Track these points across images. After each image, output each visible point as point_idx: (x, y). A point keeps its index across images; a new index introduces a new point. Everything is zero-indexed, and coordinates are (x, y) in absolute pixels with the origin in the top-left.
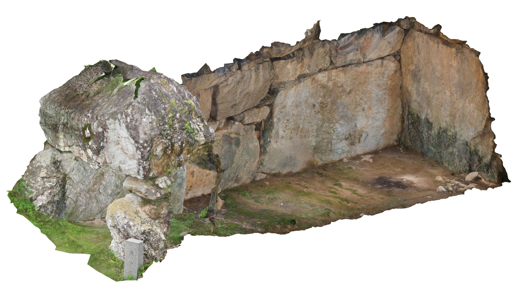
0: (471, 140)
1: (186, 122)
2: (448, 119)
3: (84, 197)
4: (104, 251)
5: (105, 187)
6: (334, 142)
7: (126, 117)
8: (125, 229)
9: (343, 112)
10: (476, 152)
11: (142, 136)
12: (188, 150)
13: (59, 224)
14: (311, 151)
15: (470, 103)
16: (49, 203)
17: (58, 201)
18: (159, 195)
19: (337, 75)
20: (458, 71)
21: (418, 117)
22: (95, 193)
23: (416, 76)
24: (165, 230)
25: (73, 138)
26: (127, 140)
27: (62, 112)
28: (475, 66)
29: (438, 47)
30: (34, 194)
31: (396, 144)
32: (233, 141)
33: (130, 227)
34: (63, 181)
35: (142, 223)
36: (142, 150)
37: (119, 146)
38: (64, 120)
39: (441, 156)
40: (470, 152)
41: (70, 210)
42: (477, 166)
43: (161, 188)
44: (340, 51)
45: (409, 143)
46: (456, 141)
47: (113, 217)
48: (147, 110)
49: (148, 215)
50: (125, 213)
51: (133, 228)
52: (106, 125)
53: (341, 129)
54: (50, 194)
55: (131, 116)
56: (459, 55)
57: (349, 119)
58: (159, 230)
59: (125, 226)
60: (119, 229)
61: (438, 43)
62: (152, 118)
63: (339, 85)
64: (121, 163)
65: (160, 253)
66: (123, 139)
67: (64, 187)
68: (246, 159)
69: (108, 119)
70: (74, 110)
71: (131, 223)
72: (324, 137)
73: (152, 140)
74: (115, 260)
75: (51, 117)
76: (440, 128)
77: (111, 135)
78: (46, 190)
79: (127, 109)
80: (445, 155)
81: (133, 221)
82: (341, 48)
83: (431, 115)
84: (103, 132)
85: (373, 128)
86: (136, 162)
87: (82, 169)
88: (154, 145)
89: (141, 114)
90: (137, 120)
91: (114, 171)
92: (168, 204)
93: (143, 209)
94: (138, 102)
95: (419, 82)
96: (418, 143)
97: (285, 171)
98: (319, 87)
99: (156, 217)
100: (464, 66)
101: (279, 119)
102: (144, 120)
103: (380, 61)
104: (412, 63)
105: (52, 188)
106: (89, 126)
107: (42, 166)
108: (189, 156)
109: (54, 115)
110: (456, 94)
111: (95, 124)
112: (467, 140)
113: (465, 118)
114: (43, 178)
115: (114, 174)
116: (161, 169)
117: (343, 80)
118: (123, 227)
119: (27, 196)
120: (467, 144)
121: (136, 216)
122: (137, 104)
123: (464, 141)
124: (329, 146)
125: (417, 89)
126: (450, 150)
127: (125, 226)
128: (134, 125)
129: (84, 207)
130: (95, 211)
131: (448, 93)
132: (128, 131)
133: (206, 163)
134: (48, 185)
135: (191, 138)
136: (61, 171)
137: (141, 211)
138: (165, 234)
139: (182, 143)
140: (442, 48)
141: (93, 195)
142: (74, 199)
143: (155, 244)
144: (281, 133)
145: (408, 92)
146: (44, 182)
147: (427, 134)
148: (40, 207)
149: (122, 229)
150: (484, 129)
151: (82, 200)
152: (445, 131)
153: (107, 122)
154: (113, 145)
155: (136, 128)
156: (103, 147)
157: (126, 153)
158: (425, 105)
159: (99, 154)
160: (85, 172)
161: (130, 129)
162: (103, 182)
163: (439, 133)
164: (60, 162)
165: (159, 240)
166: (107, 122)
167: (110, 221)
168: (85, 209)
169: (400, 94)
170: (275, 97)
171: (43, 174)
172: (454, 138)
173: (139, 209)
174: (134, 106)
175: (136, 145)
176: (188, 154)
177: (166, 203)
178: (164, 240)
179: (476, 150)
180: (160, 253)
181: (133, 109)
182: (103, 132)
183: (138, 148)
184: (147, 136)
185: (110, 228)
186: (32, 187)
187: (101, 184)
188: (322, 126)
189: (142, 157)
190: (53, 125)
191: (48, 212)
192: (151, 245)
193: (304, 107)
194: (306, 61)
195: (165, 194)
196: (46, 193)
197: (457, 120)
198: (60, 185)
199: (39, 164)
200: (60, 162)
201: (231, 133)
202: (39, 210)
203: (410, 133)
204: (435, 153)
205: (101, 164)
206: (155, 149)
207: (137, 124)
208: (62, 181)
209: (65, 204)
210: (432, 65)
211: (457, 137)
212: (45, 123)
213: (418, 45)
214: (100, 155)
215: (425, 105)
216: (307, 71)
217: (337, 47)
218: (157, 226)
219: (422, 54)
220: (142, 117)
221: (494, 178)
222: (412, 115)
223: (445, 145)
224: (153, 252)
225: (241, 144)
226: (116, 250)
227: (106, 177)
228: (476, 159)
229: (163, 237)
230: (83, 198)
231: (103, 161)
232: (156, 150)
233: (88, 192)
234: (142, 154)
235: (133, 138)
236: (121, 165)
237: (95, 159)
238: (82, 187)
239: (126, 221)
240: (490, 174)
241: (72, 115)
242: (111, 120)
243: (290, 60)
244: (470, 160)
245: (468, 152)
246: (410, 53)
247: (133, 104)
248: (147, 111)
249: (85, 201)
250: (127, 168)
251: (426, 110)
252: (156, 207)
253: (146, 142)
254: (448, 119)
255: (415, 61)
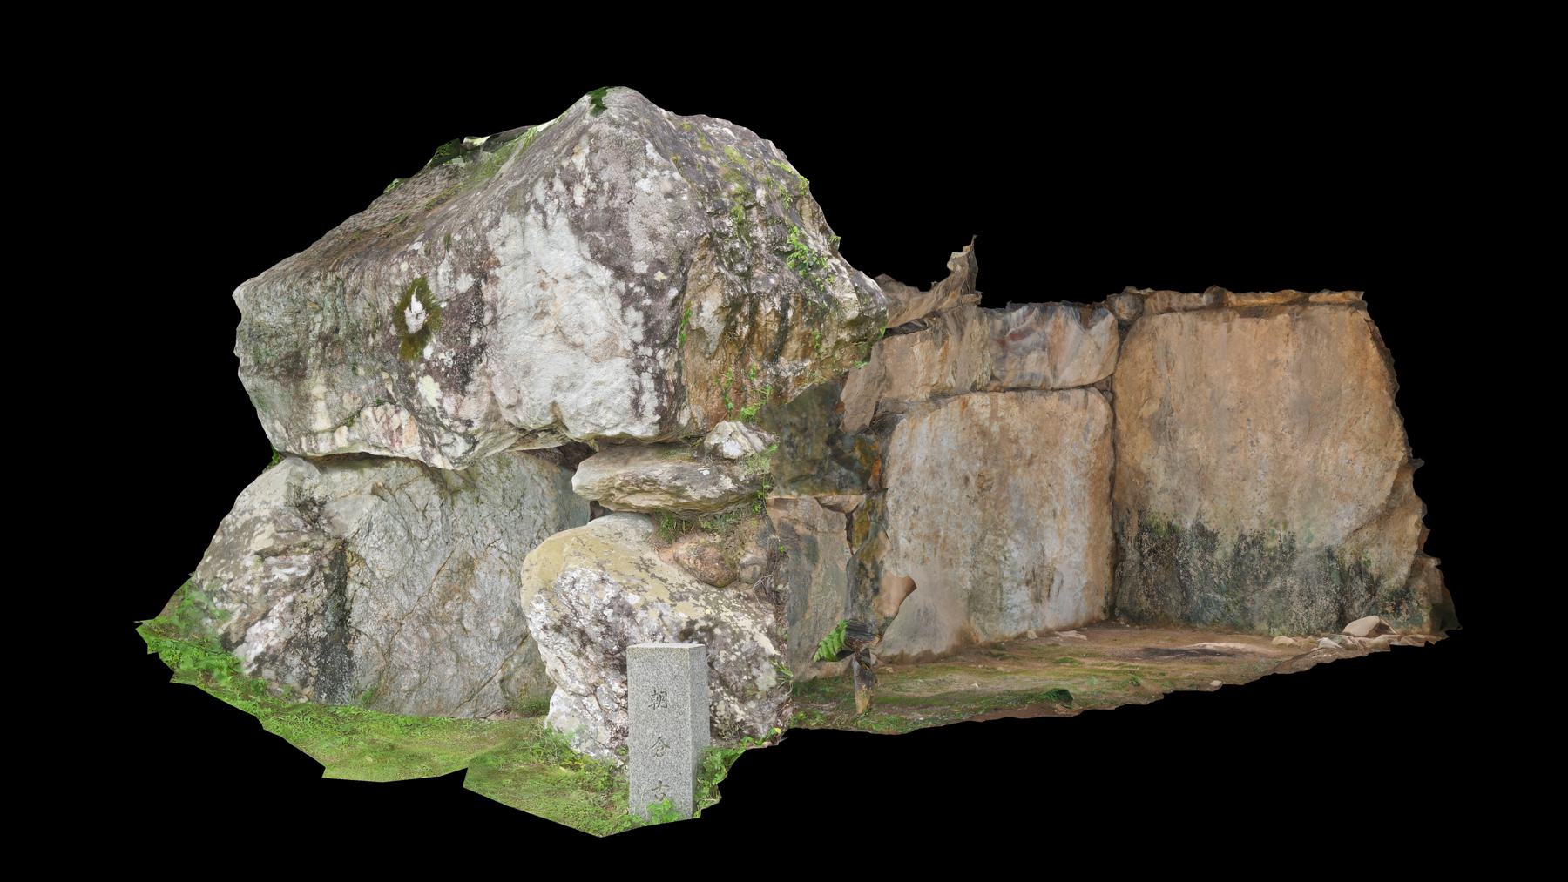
0: (1346, 539)
1: (788, 229)
2: (1266, 508)
3: (415, 640)
4: (526, 740)
5: (480, 613)
6: (1006, 586)
7: (568, 185)
8: (608, 627)
9: (1019, 510)
10: (1360, 569)
11: (641, 244)
12: (805, 338)
13: (333, 714)
14: (963, 604)
15: (1335, 444)
16: (290, 644)
17: (323, 641)
18: (728, 484)
19: (1008, 409)
20: (1299, 371)
21: (1171, 529)
22: (448, 628)
23: (1161, 429)
24: (770, 620)
25: (361, 371)
26: (579, 283)
27: (316, 291)
28: (1351, 341)
29: (1229, 330)
30: (235, 618)
31: (1103, 617)
32: (802, 545)
33: (630, 614)
34: (338, 565)
35: (672, 597)
36: (648, 302)
37: (547, 320)
38: (320, 323)
39: (1246, 609)
40: (1341, 573)
41: (368, 678)
42: (1363, 605)
43: (733, 461)
44: (1011, 343)
45: (1144, 603)
46: (1293, 558)
47: (549, 591)
48: (650, 146)
49: (690, 571)
50: (599, 565)
51: (641, 614)
52: (487, 254)
53: (1018, 555)
54: (292, 608)
55: (587, 180)
56: (1301, 325)
57: (1033, 534)
58: (745, 622)
59: (608, 612)
60: (582, 633)
61: (1227, 320)
62: (672, 179)
63: (1012, 436)
64: (558, 387)
65: (766, 710)
66: (563, 285)
67: (341, 589)
68: (835, 599)
69: (496, 223)
70: (356, 261)
71: (633, 599)
72: (988, 569)
73: (683, 261)
74: (574, 768)
75: (277, 336)
76: (1243, 537)
77: (510, 287)
78: (276, 598)
79: (571, 153)
80: (1259, 604)
81: (637, 590)
82: (1013, 336)
83: (1212, 513)
84: (477, 290)
85: (1069, 566)
86: (621, 363)
87: (401, 533)
88: (691, 285)
89: (630, 165)
90: (613, 188)
91: (505, 556)
92: (764, 525)
93: (669, 553)
94: (612, 122)
95: (1172, 439)
96: (1174, 597)
97: (916, 650)
98: (975, 430)
99: (727, 579)
100: (1315, 352)
101: (897, 502)
102: (644, 185)
103: (1081, 393)
104: (1150, 396)
105: (296, 584)
106: (421, 288)
107: (258, 519)
108: (808, 363)
109: (288, 320)
110: (1291, 433)
111: (444, 269)
112: (1329, 543)
113: (1320, 490)
114: (262, 555)
115: (505, 568)
116: (716, 401)
117: (1019, 426)
118: (599, 620)
119: (209, 631)
120: (1330, 554)
121: (643, 574)
122: (606, 128)
123: (1318, 549)
124: (998, 595)
125: (1168, 459)
126: (1276, 583)
127: (608, 612)
128: (606, 210)
129: (416, 675)
130: (453, 694)
131: (1265, 439)
132: (581, 239)
133: (822, 469)
134: (281, 574)
135: (814, 287)
136: (328, 530)
137: (658, 562)
138: (770, 634)
139: (785, 305)
140: (1243, 327)
141: (443, 636)
142: (382, 641)
143: (740, 674)
144: (903, 542)
145: (1139, 474)
146: (268, 568)
147: (1199, 564)
148: (260, 660)
149: (594, 631)
150: (1389, 499)
151: (409, 649)
152: (1257, 542)
153: (493, 236)
154: (522, 323)
155: (613, 222)
156: (482, 346)
157: (575, 346)
158: (1191, 492)
159: (469, 380)
160: (410, 548)
161: (591, 229)
162: (472, 591)
163: (1237, 552)
164: (322, 504)
165: (755, 658)
166: (493, 236)
167: (541, 607)
168: (420, 684)
169: (1117, 493)
170: (890, 434)
171: (262, 541)
172: (1289, 550)
173: (650, 555)
174: (596, 136)
175: (621, 285)
176: (804, 357)
177: (753, 522)
178: (772, 658)
179: (1358, 563)
180: (766, 710)
181: (594, 151)
182: (477, 290)
183: (628, 299)
184: (660, 246)
185: (542, 636)
186: (225, 596)
187: (466, 597)
188: (982, 539)
189: (650, 333)
190: (287, 357)
191: (292, 680)
192: (724, 683)
193: (946, 478)
194: (952, 341)
195: (754, 482)
196: (277, 608)
197: (1291, 502)
198: (328, 579)
199: (247, 516)
200: (322, 504)
201: (796, 521)
202: (257, 673)
203: (1145, 579)
204: (1226, 606)
205: (477, 424)
206: (695, 305)
207: (616, 203)
208: (332, 565)
209: (350, 654)
210: (1209, 385)
211: (1298, 545)
212: (258, 363)
213: (1167, 347)
214: (470, 387)
215: (1191, 492)
216: (950, 381)
217: (1003, 332)
218: (734, 609)
219: (1179, 366)
220: (634, 172)
221: (1420, 624)
222: (1151, 530)
223: (1257, 577)
224: (736, 707)
225: (821, 559)
226: (577, 723)
227: (481, 573)
228: (1360, 587)
229: (770, 649)
230: (409, 642)
231: (484, 408)
232: (700, 307)
233: (427, 620)
234: (647, 317)
235: (606, 261)
236: (559, 398)
237: (450, 410)
238: (404, 600)
239: (609, 593)
240: (1404, 616)
241: (353, 281)
242: (508, 221)
243: (918, 334)
244: (1342, 593)
245: (1335, 575)
246: (1144, 375)
247: (593, 129)
248: (651, 152)
249: (416, 655)
250: (587, 401)
251: (1197, 503)
252: (718, 539)
253: (660, 265)
254: (1266, 508)
255: (1159, 389)
